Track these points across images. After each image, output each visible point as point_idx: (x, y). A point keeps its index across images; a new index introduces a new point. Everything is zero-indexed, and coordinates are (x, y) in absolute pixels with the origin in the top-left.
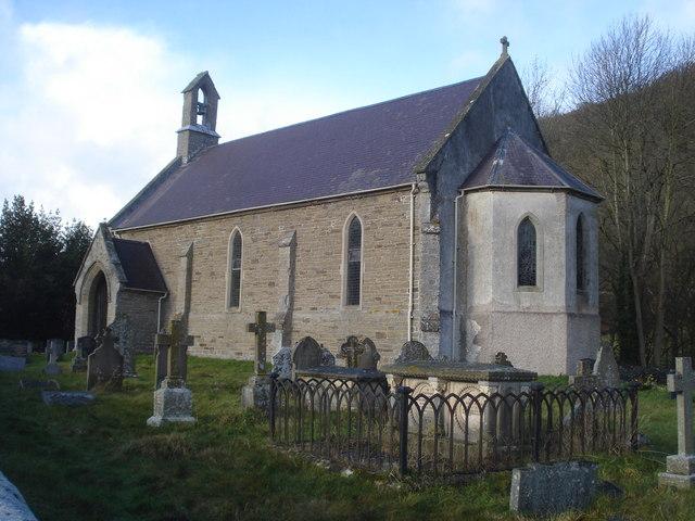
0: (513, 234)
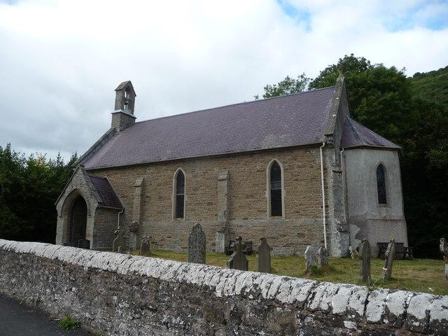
0: (374, 174)
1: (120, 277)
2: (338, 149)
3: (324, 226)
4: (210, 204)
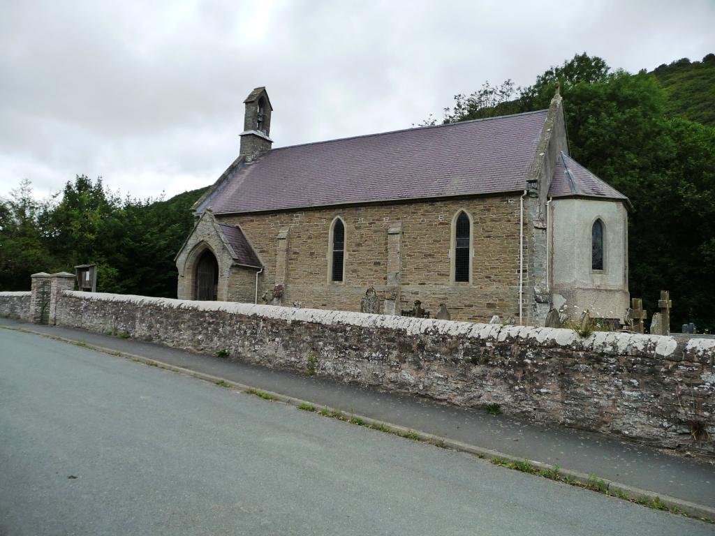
1: (324, 326)
2: (543, 199)
3: (521, 295)
4: (377, 264)
